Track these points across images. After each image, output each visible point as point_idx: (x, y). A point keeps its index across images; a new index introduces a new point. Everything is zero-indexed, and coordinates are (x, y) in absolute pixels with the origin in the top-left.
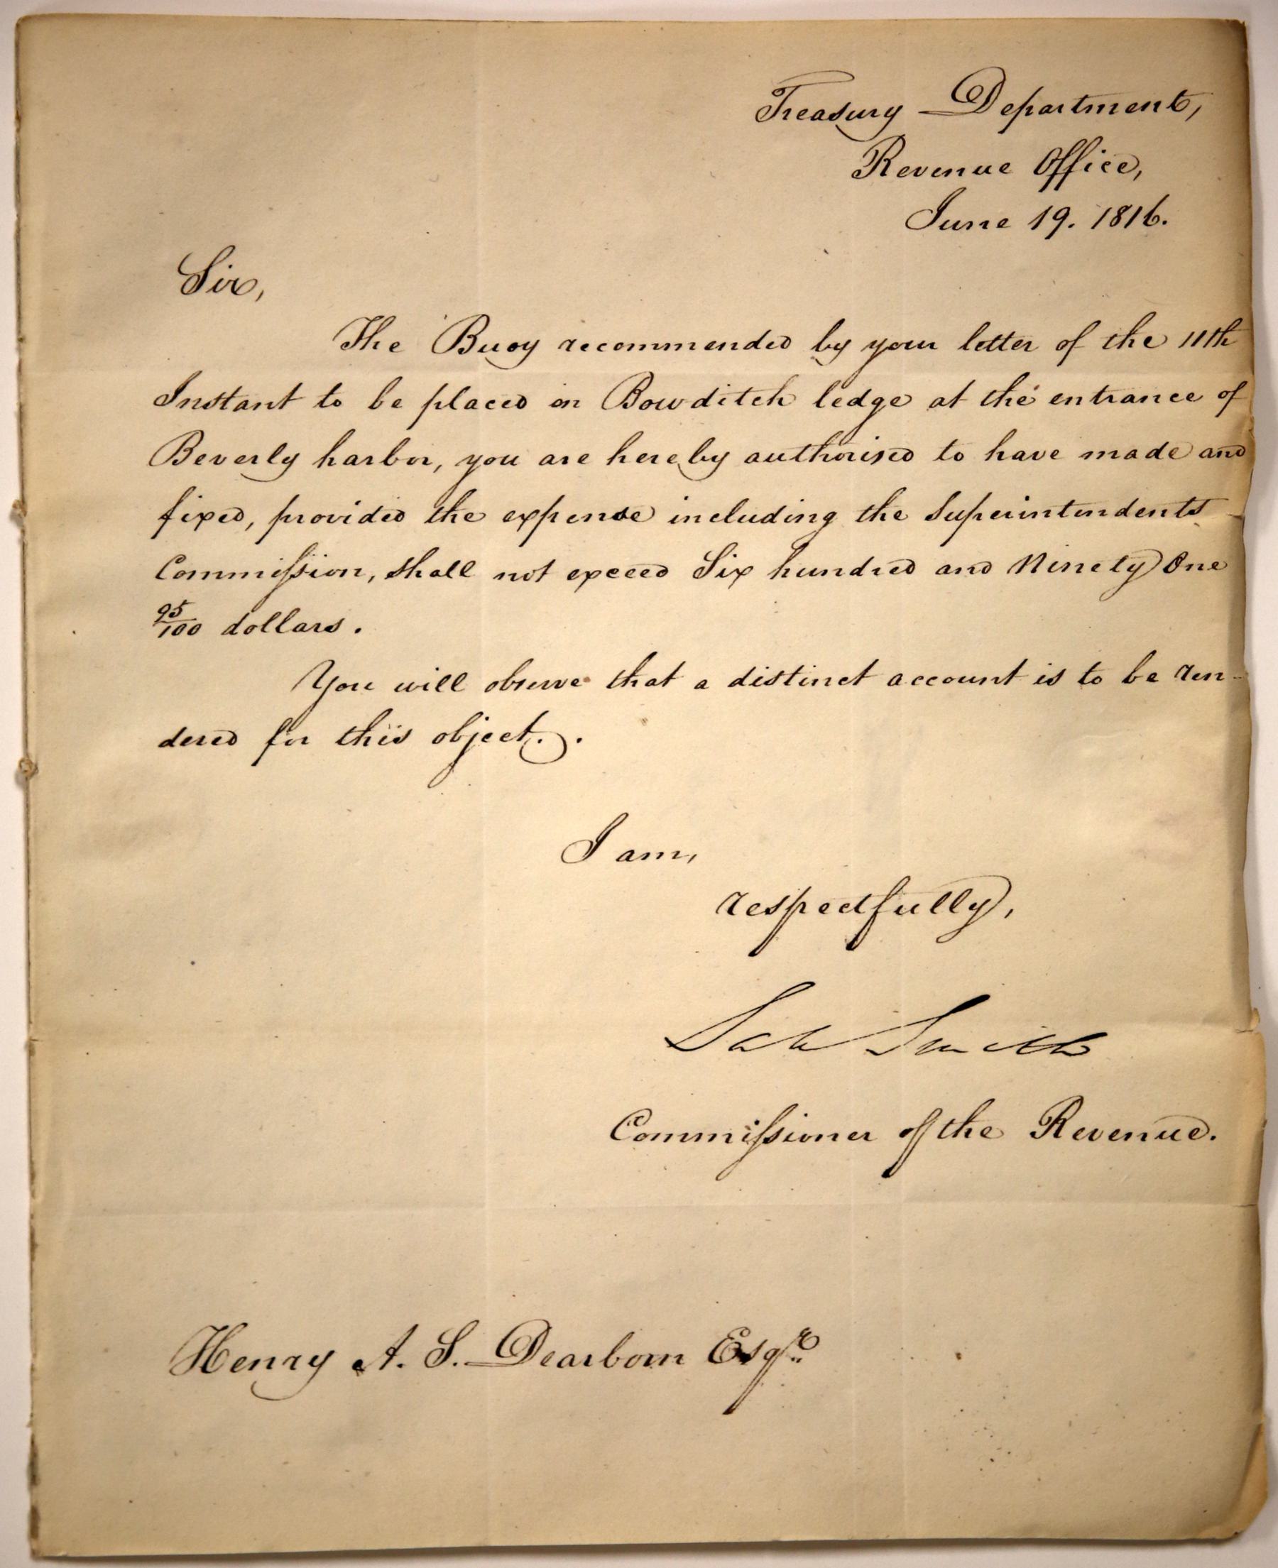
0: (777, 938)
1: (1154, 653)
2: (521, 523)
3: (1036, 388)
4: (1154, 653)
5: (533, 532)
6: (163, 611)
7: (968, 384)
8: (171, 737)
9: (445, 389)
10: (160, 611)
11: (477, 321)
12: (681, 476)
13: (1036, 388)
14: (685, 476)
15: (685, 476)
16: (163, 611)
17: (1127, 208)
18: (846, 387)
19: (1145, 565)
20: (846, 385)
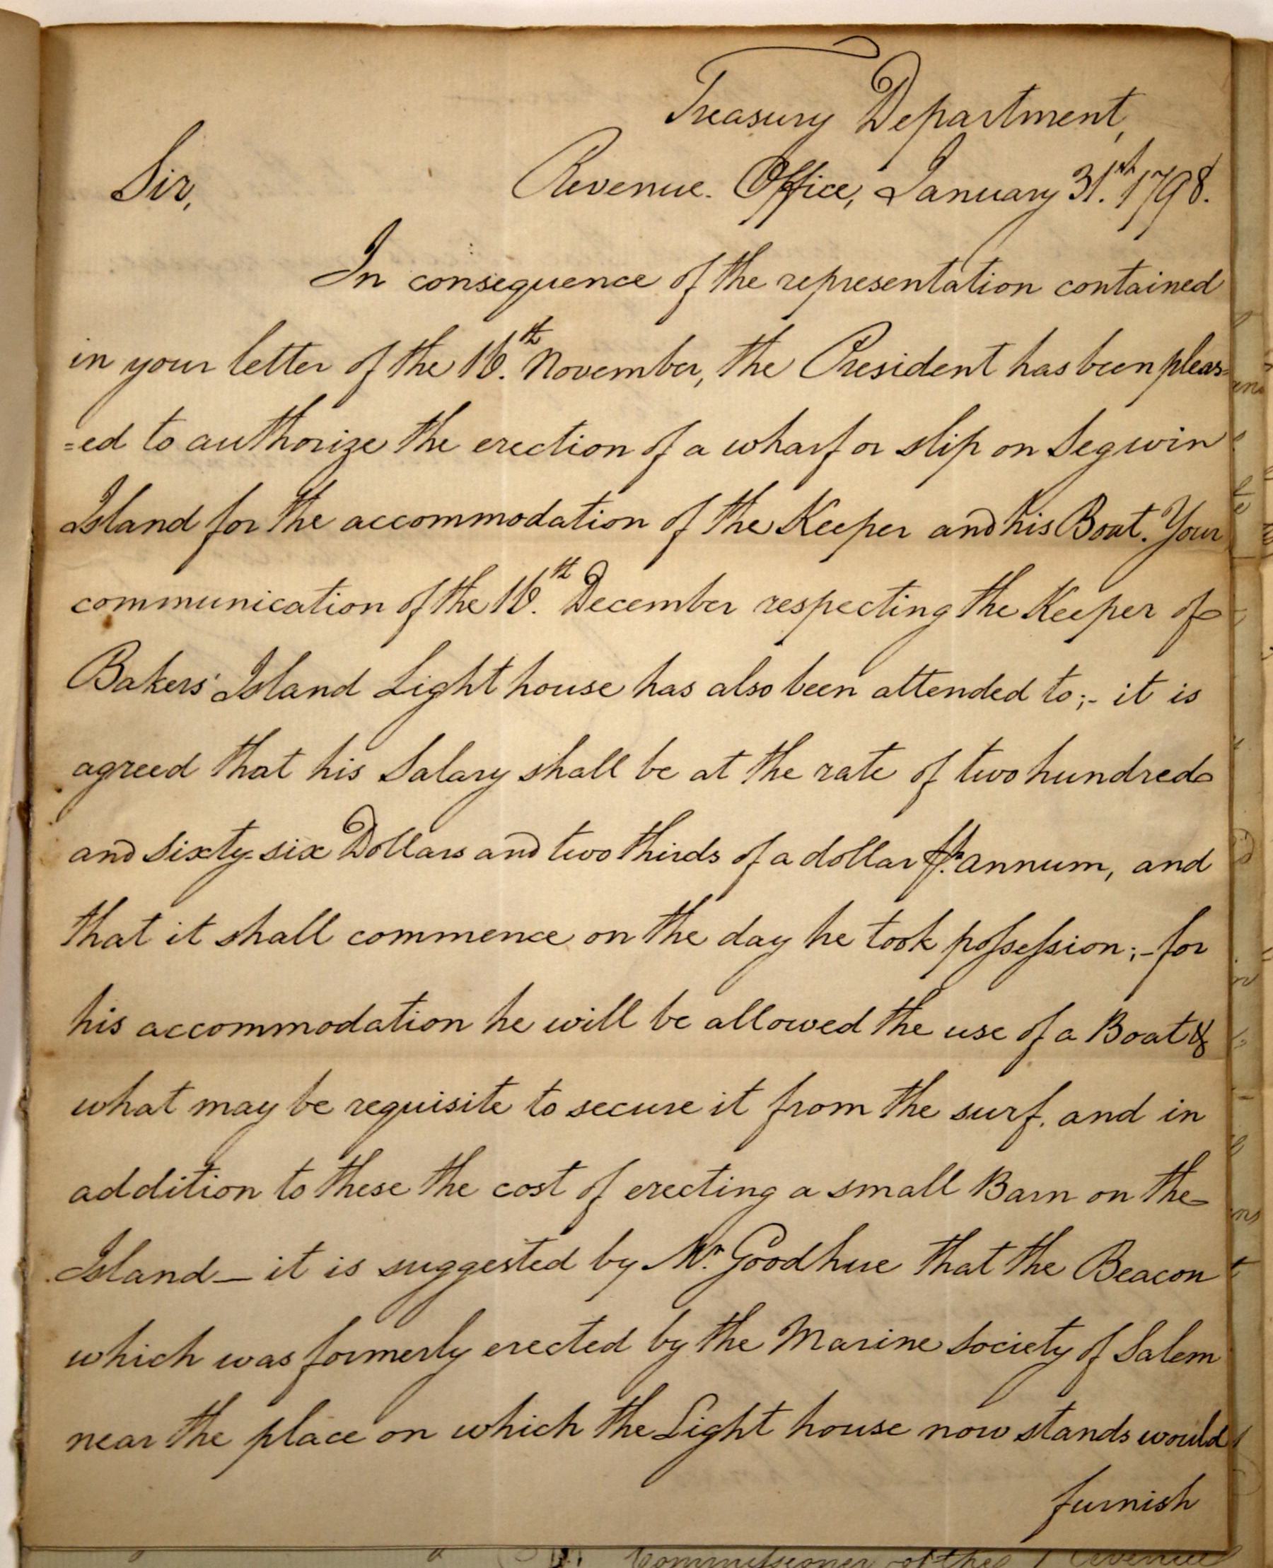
6: (102, 771)
16: (102, 771)
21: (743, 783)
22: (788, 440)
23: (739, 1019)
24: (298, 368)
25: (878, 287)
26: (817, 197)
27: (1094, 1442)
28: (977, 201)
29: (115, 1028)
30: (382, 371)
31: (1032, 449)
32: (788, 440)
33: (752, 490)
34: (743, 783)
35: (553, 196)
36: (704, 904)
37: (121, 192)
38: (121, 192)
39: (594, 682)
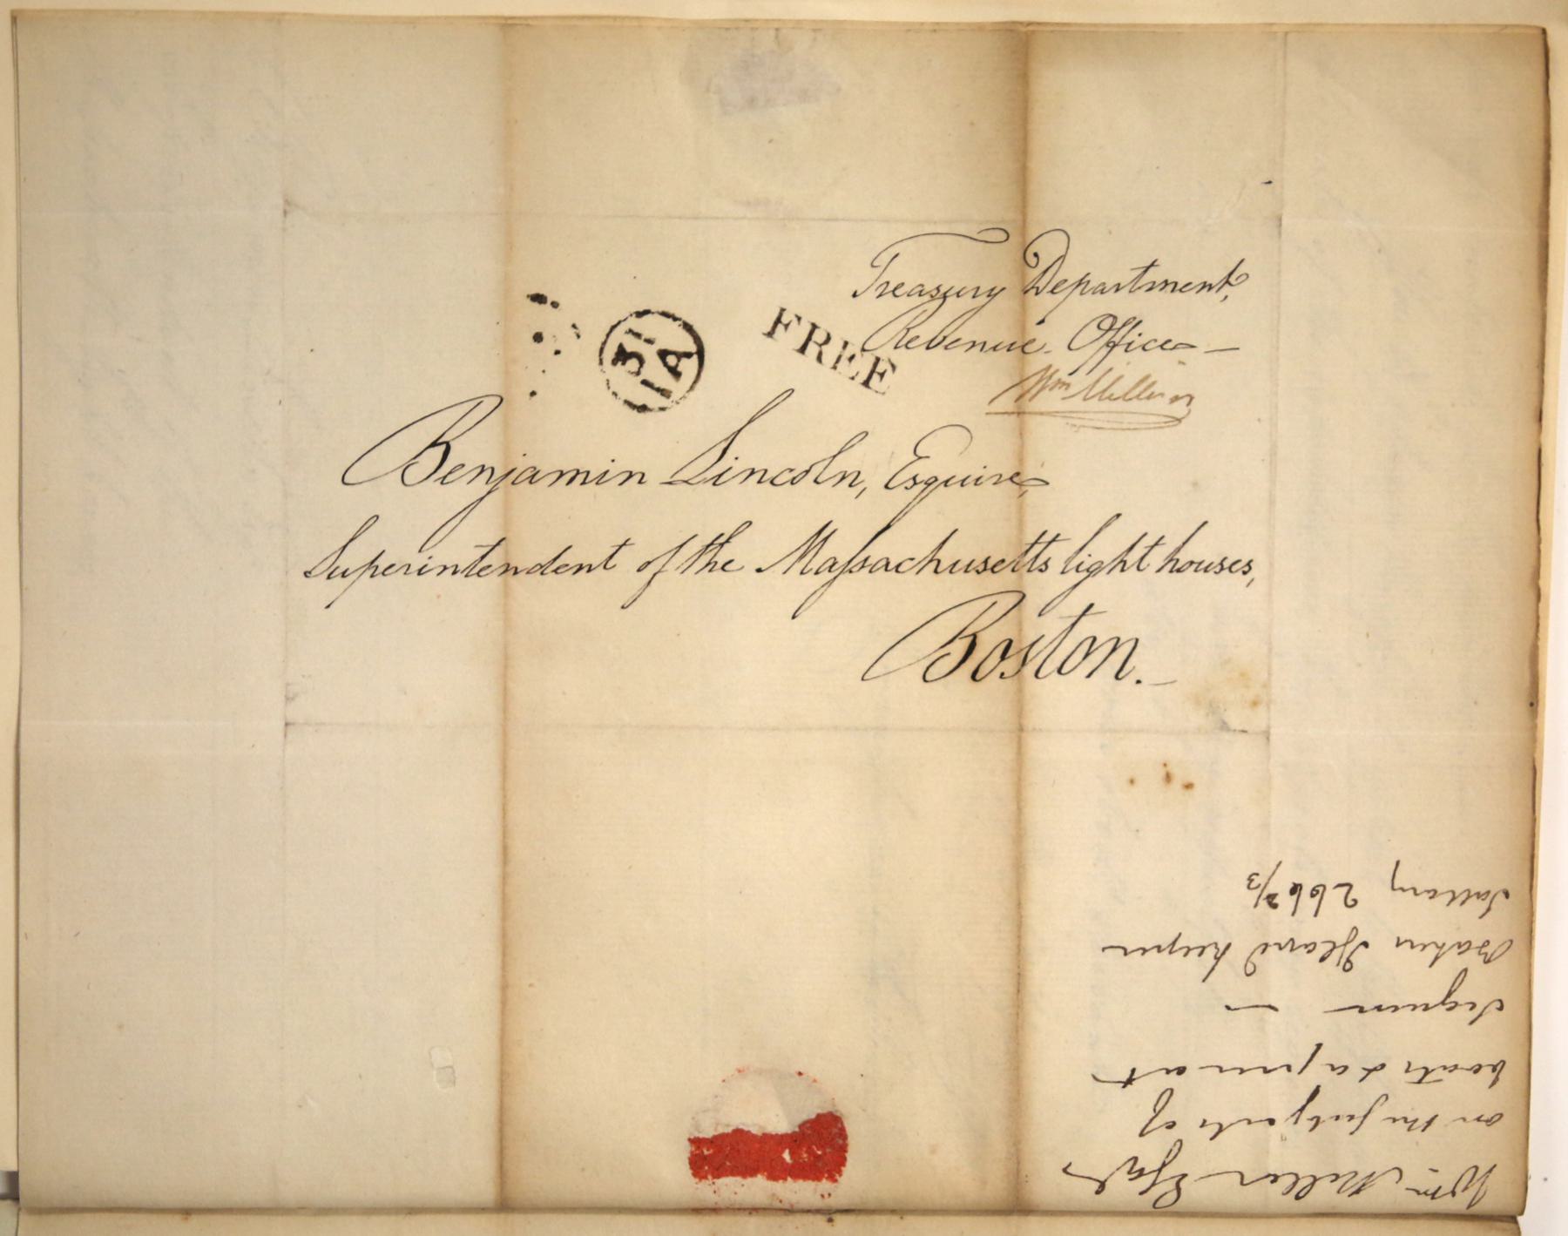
0: (26, 589)
1: (1118, 515)
2: (982, 633)
3: (430, 558)
4: (1118, 515)
5: (459, 421)
6: (1091, 570)
7: (950, 532)
8: (544, 561)
9: (569, 551)
11: (488, 553)
12: (967, 426)
13: (430, 558)
14: (961, 426)
15: (961, 426)
16: (1091, 570)
17: (906, 488)
18: (373, 517)
19: (571, 549)
20: (373, 521)
21: (1270, 182)
22: (946, 557)
23: (720, 476)
24: (481, 570)
25: (985, 569)
26: (1147, 948)
27: (1175, 574)
28: (951, 572)
29: (1043, 567)
30: (671, 573)
31: (516, 568)
32: (946, 557)
33: (917, 573)
34: (1270, 182)
35: (802, 573)
36: (798, 606)
37: (310, 573)
38: (310, 573)
39: (1225, 558)
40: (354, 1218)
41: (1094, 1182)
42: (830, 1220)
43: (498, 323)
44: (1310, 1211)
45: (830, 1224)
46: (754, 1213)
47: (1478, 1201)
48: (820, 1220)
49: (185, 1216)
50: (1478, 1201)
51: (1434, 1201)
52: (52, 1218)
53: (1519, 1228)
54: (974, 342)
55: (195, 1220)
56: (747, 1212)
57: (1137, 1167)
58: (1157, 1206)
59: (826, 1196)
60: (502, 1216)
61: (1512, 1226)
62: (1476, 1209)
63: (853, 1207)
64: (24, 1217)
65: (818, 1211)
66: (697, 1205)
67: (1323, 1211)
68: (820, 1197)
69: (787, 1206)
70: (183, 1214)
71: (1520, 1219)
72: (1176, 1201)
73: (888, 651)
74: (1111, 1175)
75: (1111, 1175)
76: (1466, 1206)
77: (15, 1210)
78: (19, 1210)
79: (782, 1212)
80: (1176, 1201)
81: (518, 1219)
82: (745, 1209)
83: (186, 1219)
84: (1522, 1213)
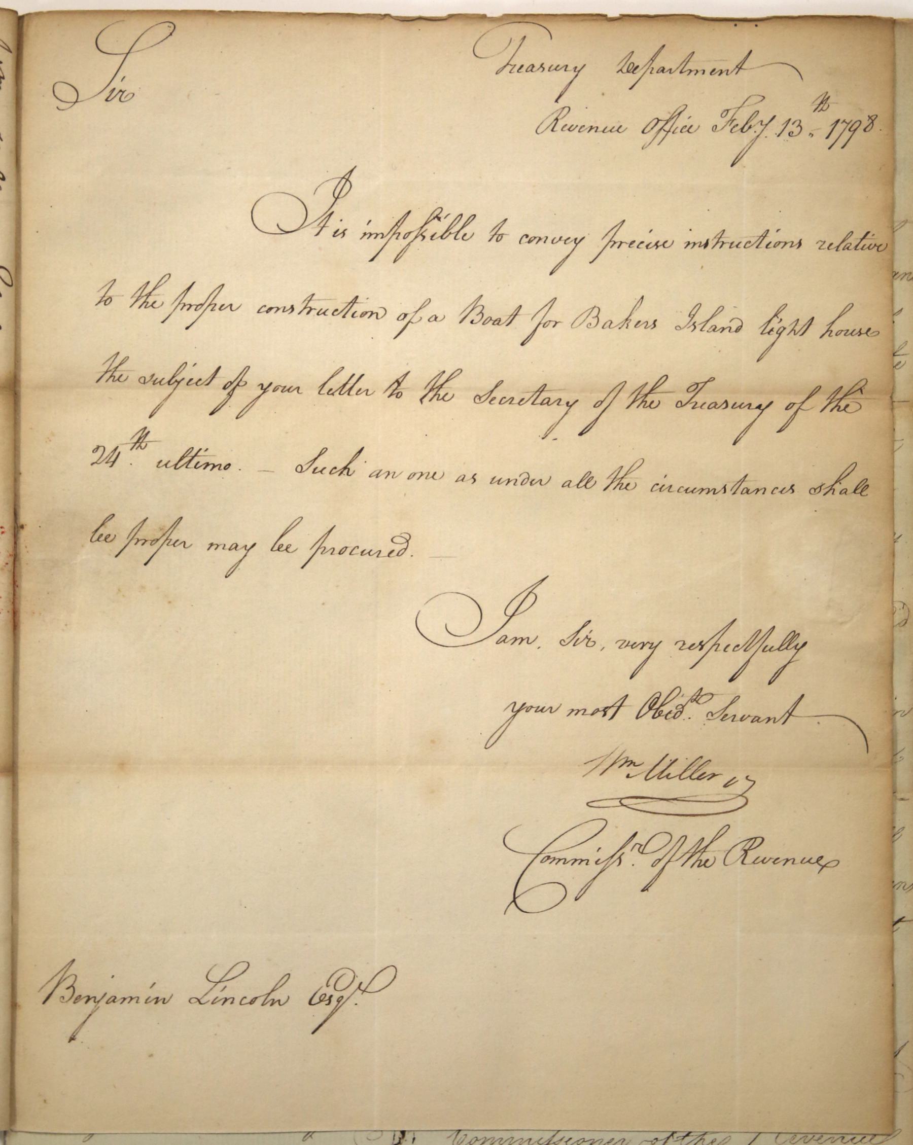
6: (779, 332)
10: (689, 316)
40: (20, 881)
41: (511, 905)
42: (22, 527)
43: (419, 30)
44: (14, 170)
45: (25, 527)
46: (17, 584)
47: (5, 44)
48: (23, 534)
49: (17, 1007)
50: (5, 44)
51: (5, 77)
52: (19, 1106)
53: (27, 15)
54: (689, 242)
55: (20, 1000)
56: (17, 589)
57: (76, 995)
58: (10, 284)
59: (3, 530)
60: (19, 771)
61: (26, 18)
62: (12, 45)
63: (12, 511)
64: (19, 1126)
65: (16, 536)
66: (10, 626)
67: (14, 160)
68: (3, 535)
69: (11, 559)
70: (16, 1009)
71: (20, 14)
72: (6, 269)
73: (638, 81)
74: (757, 103)
75: (757, 103)
76: (9, 53)
77: (13, 1133)
78: (12, 1131)
79: (17, 563)
80: (6, 269)
81: (22, 760)
82: (14, 591)
83: (19, 1006)
84: (16, 12)
